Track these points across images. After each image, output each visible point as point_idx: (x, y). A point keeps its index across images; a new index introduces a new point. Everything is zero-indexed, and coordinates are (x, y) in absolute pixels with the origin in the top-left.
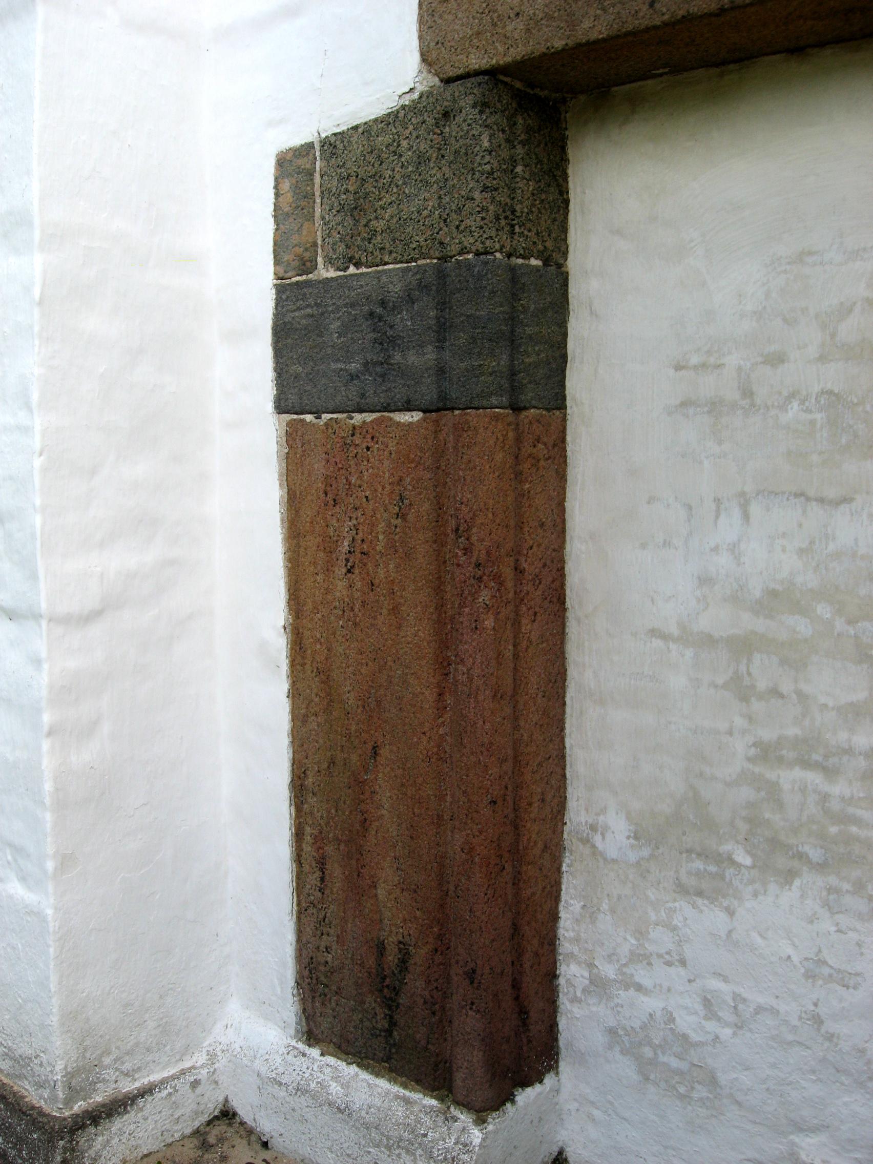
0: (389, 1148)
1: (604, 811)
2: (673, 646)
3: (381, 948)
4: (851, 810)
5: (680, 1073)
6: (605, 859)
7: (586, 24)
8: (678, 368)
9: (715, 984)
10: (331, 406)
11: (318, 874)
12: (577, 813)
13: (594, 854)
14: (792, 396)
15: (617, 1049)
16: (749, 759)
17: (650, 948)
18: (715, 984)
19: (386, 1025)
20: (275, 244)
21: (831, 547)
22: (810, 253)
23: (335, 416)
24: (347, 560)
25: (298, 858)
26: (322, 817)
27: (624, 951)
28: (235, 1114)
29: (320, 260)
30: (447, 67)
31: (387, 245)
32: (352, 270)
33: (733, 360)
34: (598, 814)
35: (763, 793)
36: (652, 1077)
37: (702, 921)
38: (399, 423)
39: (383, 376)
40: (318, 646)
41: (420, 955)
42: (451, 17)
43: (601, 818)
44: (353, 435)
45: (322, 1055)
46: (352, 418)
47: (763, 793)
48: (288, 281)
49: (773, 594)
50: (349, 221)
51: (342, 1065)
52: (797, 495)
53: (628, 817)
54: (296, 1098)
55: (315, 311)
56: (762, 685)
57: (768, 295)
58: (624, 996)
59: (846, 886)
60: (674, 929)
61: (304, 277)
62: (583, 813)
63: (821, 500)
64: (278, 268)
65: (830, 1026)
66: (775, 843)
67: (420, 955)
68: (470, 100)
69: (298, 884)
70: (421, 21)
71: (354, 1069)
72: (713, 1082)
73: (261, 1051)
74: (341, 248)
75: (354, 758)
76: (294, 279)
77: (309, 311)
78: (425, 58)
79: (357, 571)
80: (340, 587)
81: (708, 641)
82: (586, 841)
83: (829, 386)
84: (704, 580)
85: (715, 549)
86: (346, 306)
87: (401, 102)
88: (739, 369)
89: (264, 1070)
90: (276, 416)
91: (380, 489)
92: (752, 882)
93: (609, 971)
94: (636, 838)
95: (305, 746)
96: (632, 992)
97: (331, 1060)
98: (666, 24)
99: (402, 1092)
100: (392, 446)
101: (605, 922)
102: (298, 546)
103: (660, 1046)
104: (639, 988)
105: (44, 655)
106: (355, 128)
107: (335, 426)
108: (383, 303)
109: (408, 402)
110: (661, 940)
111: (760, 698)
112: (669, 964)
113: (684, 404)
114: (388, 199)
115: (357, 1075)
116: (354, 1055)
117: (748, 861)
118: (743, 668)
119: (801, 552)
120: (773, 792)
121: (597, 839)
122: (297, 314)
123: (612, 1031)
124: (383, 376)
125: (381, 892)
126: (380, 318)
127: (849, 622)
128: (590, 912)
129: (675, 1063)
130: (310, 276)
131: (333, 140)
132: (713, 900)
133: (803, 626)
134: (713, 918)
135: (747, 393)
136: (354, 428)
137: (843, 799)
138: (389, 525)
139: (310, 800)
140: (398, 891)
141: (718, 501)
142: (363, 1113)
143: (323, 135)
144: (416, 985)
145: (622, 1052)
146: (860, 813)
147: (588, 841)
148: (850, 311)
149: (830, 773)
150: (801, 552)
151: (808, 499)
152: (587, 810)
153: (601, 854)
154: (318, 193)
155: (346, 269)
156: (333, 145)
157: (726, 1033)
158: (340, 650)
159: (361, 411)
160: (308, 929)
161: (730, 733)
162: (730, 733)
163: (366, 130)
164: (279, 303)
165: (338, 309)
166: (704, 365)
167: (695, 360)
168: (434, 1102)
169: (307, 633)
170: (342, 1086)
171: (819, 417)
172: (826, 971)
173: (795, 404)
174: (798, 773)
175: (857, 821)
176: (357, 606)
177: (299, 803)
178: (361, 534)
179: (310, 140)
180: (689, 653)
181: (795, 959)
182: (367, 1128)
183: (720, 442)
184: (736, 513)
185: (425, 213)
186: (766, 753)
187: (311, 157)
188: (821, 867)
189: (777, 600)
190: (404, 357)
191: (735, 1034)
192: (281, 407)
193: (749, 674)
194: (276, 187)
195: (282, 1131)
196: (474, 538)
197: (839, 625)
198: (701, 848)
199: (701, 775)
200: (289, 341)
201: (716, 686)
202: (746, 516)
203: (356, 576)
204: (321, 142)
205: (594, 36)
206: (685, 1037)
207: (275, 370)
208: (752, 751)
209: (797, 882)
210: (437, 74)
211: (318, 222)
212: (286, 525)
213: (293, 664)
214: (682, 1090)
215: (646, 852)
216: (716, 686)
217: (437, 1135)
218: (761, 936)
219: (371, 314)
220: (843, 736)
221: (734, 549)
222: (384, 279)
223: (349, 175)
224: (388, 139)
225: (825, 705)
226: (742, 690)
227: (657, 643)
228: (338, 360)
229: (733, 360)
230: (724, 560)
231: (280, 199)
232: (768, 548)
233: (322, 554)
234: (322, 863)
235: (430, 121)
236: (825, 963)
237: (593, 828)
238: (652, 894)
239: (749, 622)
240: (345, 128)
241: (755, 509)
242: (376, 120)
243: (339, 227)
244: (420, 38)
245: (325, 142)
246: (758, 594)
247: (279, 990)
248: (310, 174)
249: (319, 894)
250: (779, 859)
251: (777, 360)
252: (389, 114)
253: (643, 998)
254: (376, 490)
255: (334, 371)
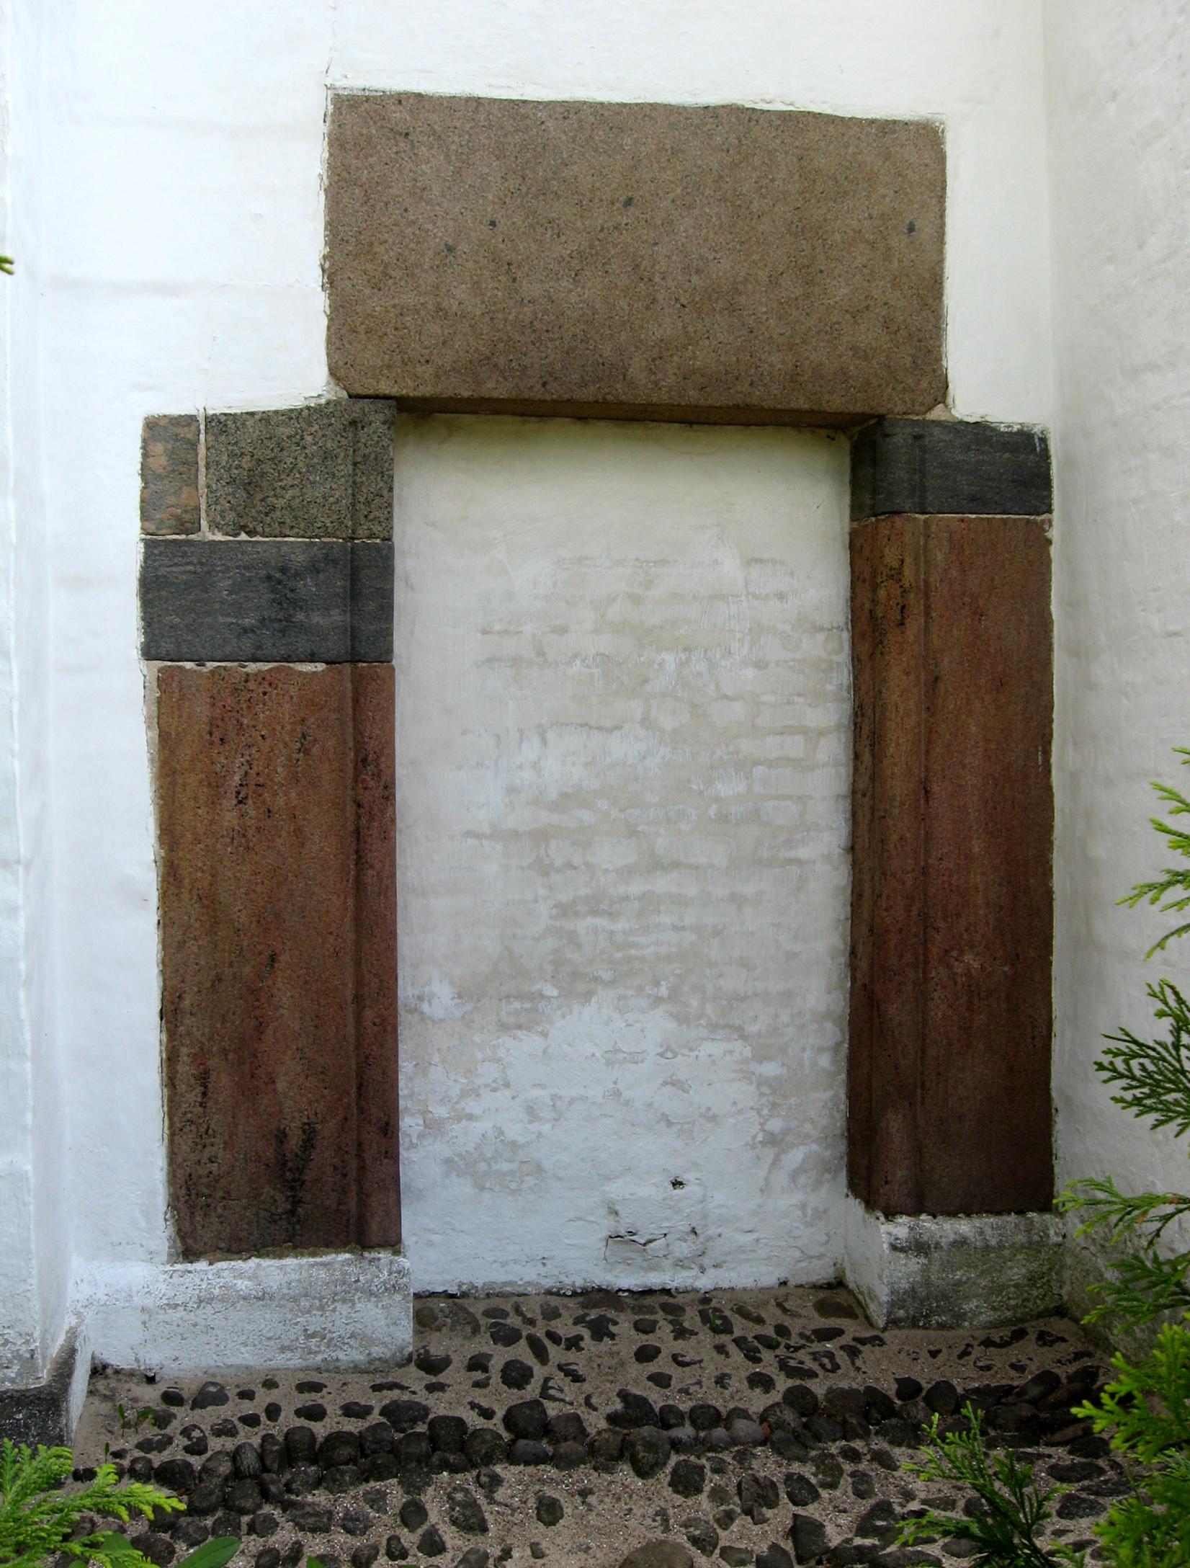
0: (321, 1308)
1: (429, 982)
2: (485, 842)
3: (281, 1137)
4: (631, 939)
5: (512, 1173)
6: (433, 1021)
7: (490, 385)
8: (485, 632)
9: (535, 1093)
10: (219, 654)
11: (200, 1089)
12: (406, 990)
13: (422, 1020)
14: (576, 656)
15: (454, 1173)
16: (551, 918)
17: (479, 1081)
18: (535, 1093)
19: (289, 1207)
20: (142, 501)
21: (608, 760)
22: (586, 558)
23: (223, 664)
24: (238, 793)
25: (171, 1081)
26: (203, 1034)
27: (455, 1091)
28: (105, 1367)
29: (204, 523)
30: (356, 385)
31: (288, 521)
32: (243, 537)
33: (528, 629)
34: (423, 986)
35: (564, 941)
36: (488, 1185)
37: (520, 1049)
38: (301, 673)
39: (283, 631)
40: (199, 874)
41: (327, 1130)
42: (360, 346)
43: (427, 989)
44: (246, 681)
45: (211, 1264)
46: (244, 667)
47: (564, 941)
48: (161, 538)
49: (565, 796)
50: (241, 494)
51: (239, 1264)
52: (582, 726)
53: (452, 983)
54: (199, 1312)
55: (199, 569)
56: (558, 862)
57: (555, 584)
58: (456, 1128)
59: (631, 992)
60: (499, 1060)
61: (183, 537)
62: (409, 988)
63: (600, 728)
64: (147, 524)
65: (627, 1095)
66: (576, 975)
67: (327, 1130)
68: (381, 417)
69: (170, 1108)
70: (329, 341)
71: (254, 1262)
72: (539, 1169)
73: (134, 1289)
74: (231, 516)
75: (247, 970)
76: (169, 537)
77: (192, 568)
78: (333, 372)
79: (250, 801)
80: (230, 818)
81: (515, 835)
82: (415, 1010)
83: (602, 650)
84: (512, 790)
85: (520, 767)
86: (237, 567)
87: (307, 403)
88: (534, 636)
89: (149, 1302)
90: (143, 663)
91: (279, 728)
92: (559, 1007)
93: (440, 1111)
94: (460, 997)
95: (181, 971)
96: (464, 1122)
97: (224, 1265)
98: (553, 401)
99: (311, 1260)
100: (293, 691)
101: (437, 1074)
102: (174, 783)
103: (492, 1158)
104: (470, 1117)
105: (21, 901)
106: (252, 414)
107: (223, 673)
108: (284, 570)
109: (313, 654)
110: (488, 1072)
111: (558, 871)
112: (495, 1090)
113: (491, 660)
114: (289, 481)
115: (259, 1265)
116: (248, 1250)
117: (555, 993)
118: (542, 852)
119: (586, 765)
120: (572, 939)
121: (425, 1007)
122: (174, 569)
123: (448, 1161)
124: (283, 631)
125: (281, 1085)
126: (279, 582)
127: (621, 811)
128: (423, 1067)
129: (506, 1167)
130: (192, 537)
131: (222, 419)
132: (529, 1029)
133: (587, 816)
134: (531, 1042)
135: (540, 653)
136: (248, 675)
137: (624, 932)
138: (289, 758)
139: (186, 1021)
140: (302, 1079)
141: (521, 731)
142: (285, 1291)
143: (210, 412)
144: (324, 1156)
145: (458, 1175)
146: (637, 939)
147: (416, 1010)
148: (614, 600)
149: (612, 915)
150: (586, 765)
151: (591, 728)
152: (413, 985)
153: (429, 1018)
154: (202, 464)
155: (239, 534)
156: (221, 425)
157: (545, 1128)
158: (230, 874)
159: (255, 660)
160: (184, 1148)
161: (536, 901)
162: (536, 901)
163: (266, 418)
164: (148, 557)
165: (228, 569)
166: (506, 632)
167: (497, 627)
168: (348, 1256)
169: (183, 864)
170: (250, 1279)
171: (595, 671)
172: (621, 1056)
173: (578, 662)
174: (590, 921)
175: (635, 945)
176: (250, 833)
177: (172, 1026)
178: (255, 769)
179: (193, 412)
180: (499, 847)
181: (598, 1055)
182: (295, 1301)
183: (521, 688)
184: (536, 742)
185: (331, 500)
186: (565, 910)
187: (193, 428)
188: (612, 983)
189: (569, 799)
190: (307, 616)
191: (553, 1126)
192: (149, 653)
193: (548, 856)
194: (143, 448)
195: (176, 1353)
196: (383, 766)
197: (614, 813)
198: (513, 993)
199: (514, 936)
200: (163, 593)
201: (523, 868)
202: (544, 742)
203: (250, 808)
204: (206, 417)
205: (495, 395)
206: (514, 1143)
207: (143, 619)
208: (554, 911)
209: (594, 999)
210: (345, 388)
211: (203, 490)
212: (157, 765)
213: (164, 896)
214: (513, 1186)
215: (469, 1007)
216: (523, 868)
217: (369, 1277)
218: (569, 1045)
219: (269, 578)
220: (621, 889)
221: (535, 766)
222: (284, 548)
223: (242, 454)
224: (289, 431)
225: (607, 870)
226: (543, 868)
227: (472, 842)
228: (228, 615)
229: (528, 629)
230: (527, 775)
231: (151, 460)
232: (560, 763)
233: (205, 790)
234: (203, 1078)
235: (338, 426)
236: (620, 1050)
237: (420, 998)
238: (477, 1039)
239: (547, 818)
240: (239, 411)
241: (551, 736)
242: (276, 412)
243: (229, 498)
244: (328, 355)
245: (209, 420)
246: (554, 796)
247: (143, 1224)
248: (193, 445)
249: (200, 1109)
250: (578, 984)
251: (564, 630)
252: (291, 411)
253: (474, 1124)
254: (274, 729)
255: (223, 624)
